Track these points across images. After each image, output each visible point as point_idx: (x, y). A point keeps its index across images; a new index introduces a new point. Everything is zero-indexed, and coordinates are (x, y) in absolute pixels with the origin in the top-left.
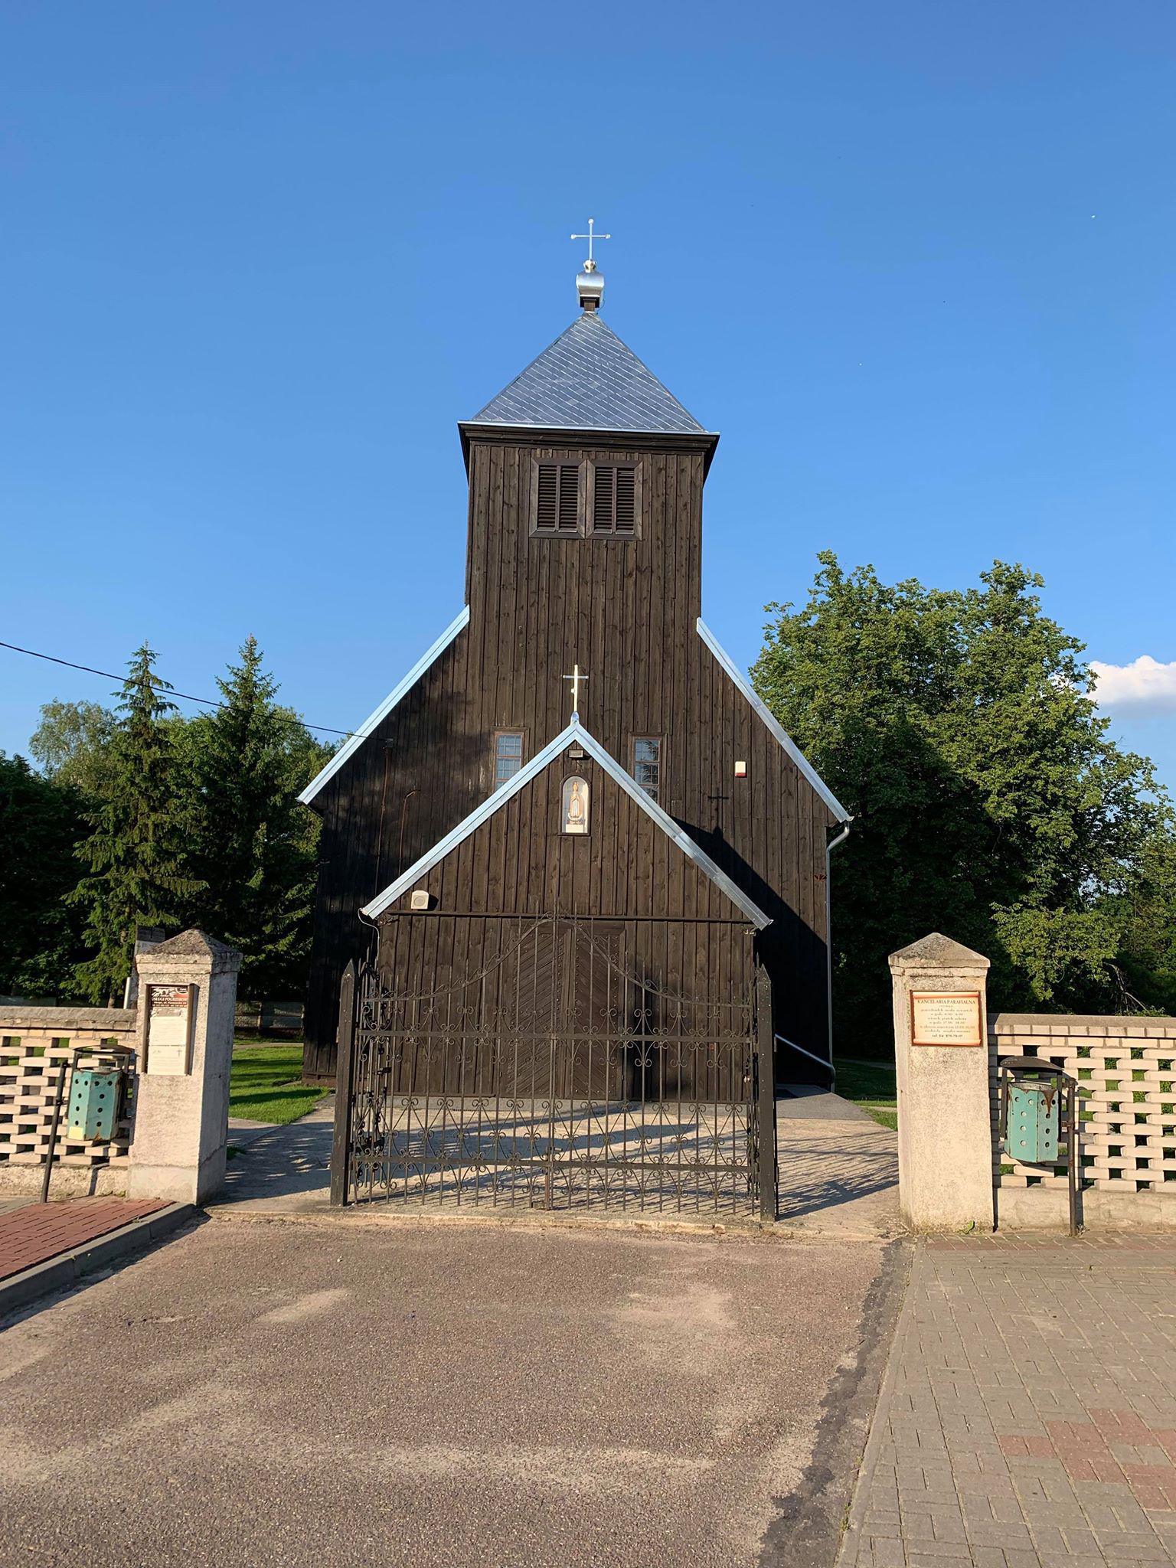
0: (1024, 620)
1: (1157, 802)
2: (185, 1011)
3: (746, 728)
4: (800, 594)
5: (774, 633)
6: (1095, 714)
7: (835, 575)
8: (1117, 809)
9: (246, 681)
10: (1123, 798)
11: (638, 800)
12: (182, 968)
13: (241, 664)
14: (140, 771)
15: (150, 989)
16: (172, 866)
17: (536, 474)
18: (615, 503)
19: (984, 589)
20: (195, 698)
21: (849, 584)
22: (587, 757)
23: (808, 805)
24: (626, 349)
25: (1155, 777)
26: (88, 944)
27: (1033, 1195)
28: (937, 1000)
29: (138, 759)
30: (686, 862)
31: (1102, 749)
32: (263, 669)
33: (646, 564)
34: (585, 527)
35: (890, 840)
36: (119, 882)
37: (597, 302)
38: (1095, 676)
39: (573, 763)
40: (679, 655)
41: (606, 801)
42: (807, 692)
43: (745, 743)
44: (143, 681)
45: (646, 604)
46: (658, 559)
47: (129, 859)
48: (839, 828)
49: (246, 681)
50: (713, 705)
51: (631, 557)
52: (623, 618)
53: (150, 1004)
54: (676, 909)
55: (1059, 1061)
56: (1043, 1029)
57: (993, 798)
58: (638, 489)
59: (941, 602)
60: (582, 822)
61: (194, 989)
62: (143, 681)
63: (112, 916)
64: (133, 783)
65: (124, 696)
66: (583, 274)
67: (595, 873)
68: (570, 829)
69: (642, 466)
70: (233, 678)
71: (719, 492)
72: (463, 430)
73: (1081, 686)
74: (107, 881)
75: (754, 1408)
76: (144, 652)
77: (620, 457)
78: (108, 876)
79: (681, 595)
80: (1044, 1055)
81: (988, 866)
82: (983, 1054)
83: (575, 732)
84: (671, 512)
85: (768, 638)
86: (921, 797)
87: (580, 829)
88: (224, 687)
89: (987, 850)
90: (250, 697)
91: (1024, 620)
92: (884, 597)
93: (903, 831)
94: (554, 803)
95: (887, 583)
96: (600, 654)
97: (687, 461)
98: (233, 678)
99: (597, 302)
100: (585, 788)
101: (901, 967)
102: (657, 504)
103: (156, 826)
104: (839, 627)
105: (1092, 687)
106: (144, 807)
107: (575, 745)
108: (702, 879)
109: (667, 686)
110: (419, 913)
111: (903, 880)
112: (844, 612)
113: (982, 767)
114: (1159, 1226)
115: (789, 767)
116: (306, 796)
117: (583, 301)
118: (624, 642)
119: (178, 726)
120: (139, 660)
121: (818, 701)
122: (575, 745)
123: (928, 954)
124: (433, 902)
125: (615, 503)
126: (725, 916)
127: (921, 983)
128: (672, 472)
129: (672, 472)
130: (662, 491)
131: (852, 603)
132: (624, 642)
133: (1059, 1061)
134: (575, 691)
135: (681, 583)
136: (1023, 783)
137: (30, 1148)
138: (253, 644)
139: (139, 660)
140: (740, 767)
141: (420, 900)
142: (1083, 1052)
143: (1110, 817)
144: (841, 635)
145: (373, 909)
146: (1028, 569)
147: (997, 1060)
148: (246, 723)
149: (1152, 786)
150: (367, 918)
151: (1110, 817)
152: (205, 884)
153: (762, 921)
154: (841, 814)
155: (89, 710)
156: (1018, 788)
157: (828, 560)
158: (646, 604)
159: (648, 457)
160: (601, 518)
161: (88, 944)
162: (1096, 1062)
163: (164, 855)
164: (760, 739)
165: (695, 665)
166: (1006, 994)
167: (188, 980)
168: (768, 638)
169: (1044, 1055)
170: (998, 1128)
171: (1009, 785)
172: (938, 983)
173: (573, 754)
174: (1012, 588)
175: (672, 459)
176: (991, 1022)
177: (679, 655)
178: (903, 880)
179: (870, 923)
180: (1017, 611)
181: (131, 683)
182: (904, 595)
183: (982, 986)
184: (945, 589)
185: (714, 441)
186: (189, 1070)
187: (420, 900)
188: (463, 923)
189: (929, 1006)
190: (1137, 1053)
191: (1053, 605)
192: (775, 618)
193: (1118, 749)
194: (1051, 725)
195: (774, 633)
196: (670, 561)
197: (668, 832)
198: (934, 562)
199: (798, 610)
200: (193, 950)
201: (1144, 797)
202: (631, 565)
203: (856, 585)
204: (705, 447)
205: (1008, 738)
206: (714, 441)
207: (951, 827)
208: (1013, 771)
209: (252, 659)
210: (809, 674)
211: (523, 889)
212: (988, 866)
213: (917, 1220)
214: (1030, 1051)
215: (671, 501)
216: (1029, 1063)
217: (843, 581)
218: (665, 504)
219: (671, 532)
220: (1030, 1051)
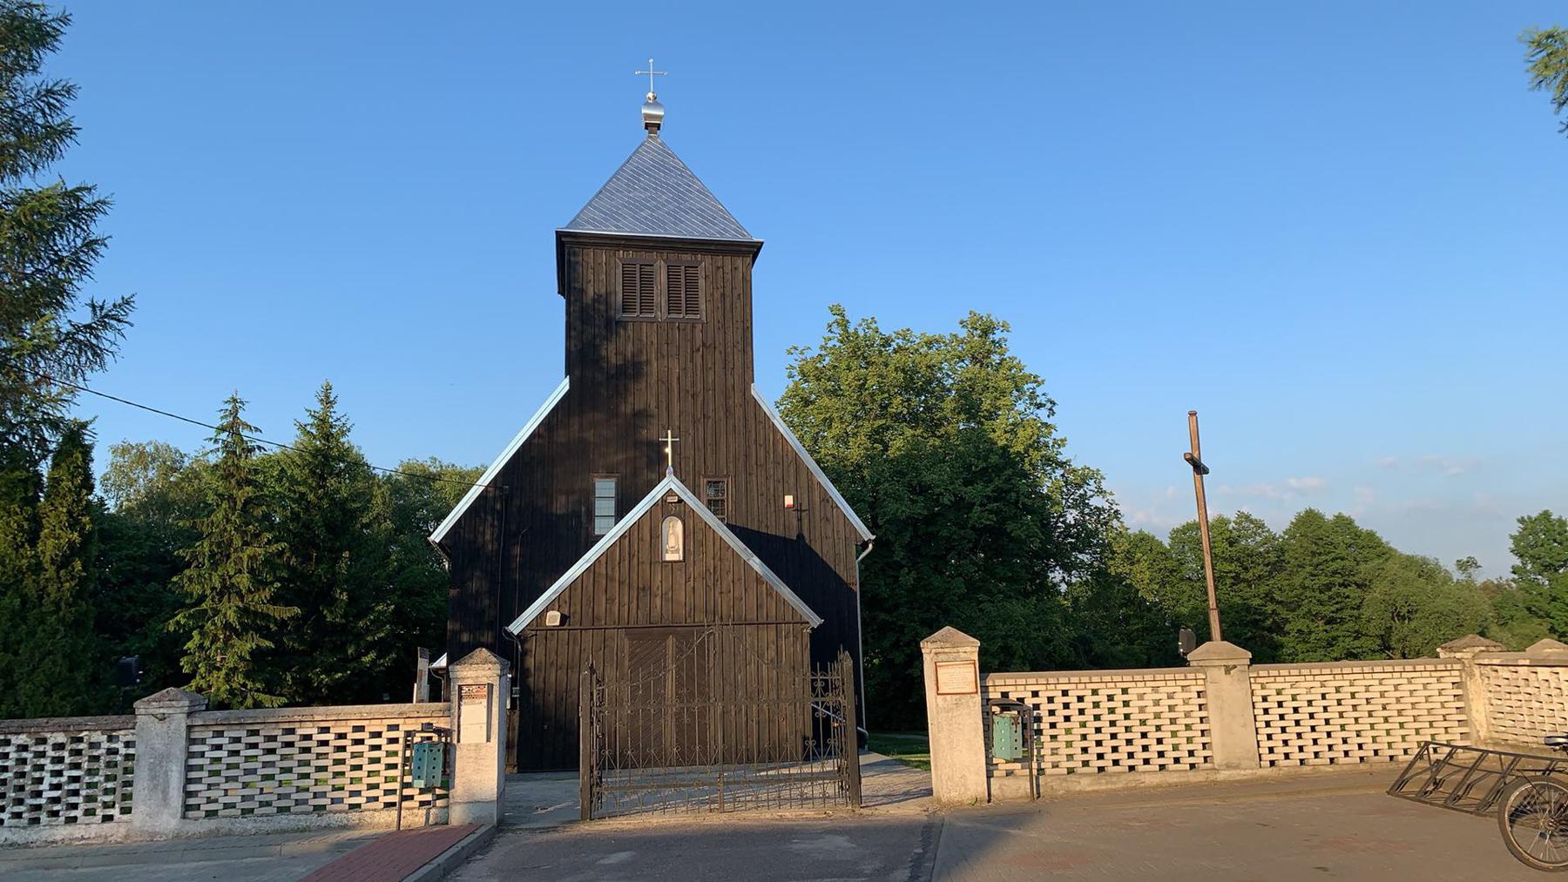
0: (996, 358)
1: (1106, 506)
2: (485, 702)
3: (792, 470)
4: (815, 338)
5: (795, 372)
6: (1055, 435)
7: (844, 324)
8: (1075, 512)
9: (323, 422)
10: (1082, 502)
11: (720, 533)
12: (481, 673)
13: (318, 408)
14: (234, 509)
15: (460, 688)
16: (266, 594)
17: (619, 271)
18: (683, 294)
19: (963, 333)
20: (278, 432)
21: (856, 332)
22: (681, 501)
23: (841, 528)
24: (685, 167)
25: (1104, 485)
26: (186, 670)
27: (1010, 781)
28: (950, 669)
29: (231, 498)
30: (758, 579)
31: (1062, 465)
32: (338, 410)
33: (710, 342)
34: (661, 314)
35: (896, 545)
36: (216, 612)
37: (658, 126)
38: (1053, 403)
39: (667, 507)
40: (739, 412)
41: (695, 534)
42: (828, 422)
43: (792, 481)
44: (233, 426)
45: (711, 373)
46: (719, 338)
47: (226, 589)
48: (865, 545)
49: (323, 422)
50: (767, 452)
51: (698, 336)
52: (694, 384)
53: (460, 698)
54: (752, 616)
55: (1021, 700)
56: (1012, 682)
57: (977, 509)
58: (701, 282)
59: (929, 344)
60: (677, 551)
61: (491, 686)
62: (233, 426)
63: (207, 643)
64: (228, 521)
65: (216, 441)
66: (647, 104)
67: (689, 589)
68: (669, 557)
69: (705, 263)
70: (311, 421)
71: (761, 272)
72: (559, 235)
73: (1043, 414)
74: (205, 611)
75: (878, 865)
76: (235, 400)
77: (687, 257)
78: (204, 606)
79: (739, 365)
80: (1013, 697)
81: (975, 564)
82: (978, 698)
83: (670, 483)
84: (728, 300)
85: (791, 376)
86: (920, 509)
87: (678, 557)
88: (303, 428)
89: (973, 551)
90: (327, 437)
91: (996, 358)
92: (887, 342)
93: (907, 537)
94: (656, 537)
95: (886, 331)
96: (676, 413)
97: (739, 261)
98: (311, 421)
99: (658, 126)
100: (679, 525)
101: (928, 648)
102: (717, 295)
103: (250, 557)
104: (849, 369)
105: (1052, 412)
106: (238, 542)
107: (670, 492)
108: (770, 592)
109: (731, 438)
110: (553, 629)
111: (907, 578)
112: (854, 354)
113: (967, 483)
114: (1080, 792)
115: (826, 498)
116: (437, 536)
117: (647, 126)
118: (695, 403)
119: (270, 462)
120: (229, 407)
121: (835, 431)
122: (670, 492)
123: (944, 640)
124: (564, 619)
125: (683, 294)
126: (789, 618)
127: (941, 657)
128: (728, 268)
129: (728, 268)
130: (720, 284)
131: (859, 349)
132: (695, 403)
133: (1021, 700)
134: (668, 450)
135: (738, 357)
136: (1000, 495)
137: (376, 799)
138: (328, 389)
139: (229, 407)
140: (789, 500)
141: (554, 618)
142: (1035, 694)
143: (1070, 519)
144: (852, 375)
145: (516, 627)
146: (997, 317)
147: (987, 702)
148: (327, 455)
149: (1100, 491)
150: (510, 634)
151: (1070, 519)
152: (297, 610)
153: (816, 621)
154: (867, 535)
155: (157, 449)
156: (996, 500)
157: (838, 311)
158: (711, 373)
159: (708, 258)
160: (673, 306)
161: (186, 670)
162: (1042, 700)
163: (258, 583)
164: (803, 478)
165: (752, 422)
166: (988, 665)
167: (485, 681)
168: (791, 376)
169: (1013, 697)
170: (988, 744)
171: (988, 498)
172: (951, 657)
173: (670, 500)
174: (985, 333)
175: (728, 259)
176: (983, 679)
177: (739, 412)
178: (907, 578)
179: (883, 616)
180: (989, 352)
181: (222, 429)
182: (900, 341)
183: (976, 657)
184: (931, 333)
185: (759, 246)
186: (488, 740)
187: (554, 617)
188: (588, 635)
189: (950, 670)
190: (1065, 693)
191: (1020, 348)
192: (794, 361)
193: (1075, 465)
194: (1021, 448)
195: (795, 372)
196: (729, 338)
197: (744, 557)
198: (918, 309)
199: (815, 352)
200: (486, 662)
201: (1096, 502)
202: (699, 342)
203: (861, 334)
204: (753, 250)
205: (986, 459)
206: (759, 246)
207: (945, 533)
208: (992, 487)
209: (328, 401)
210: (827, 408)
211: (634, 606)
212: (975, 564)
213: (944, 800)
214: (1005, 695)
215: (728, 293)
216: (1005, 701)
217: (851, 330)
218: (723, 295)
219: (728, 315)
220: (1005, 695)
